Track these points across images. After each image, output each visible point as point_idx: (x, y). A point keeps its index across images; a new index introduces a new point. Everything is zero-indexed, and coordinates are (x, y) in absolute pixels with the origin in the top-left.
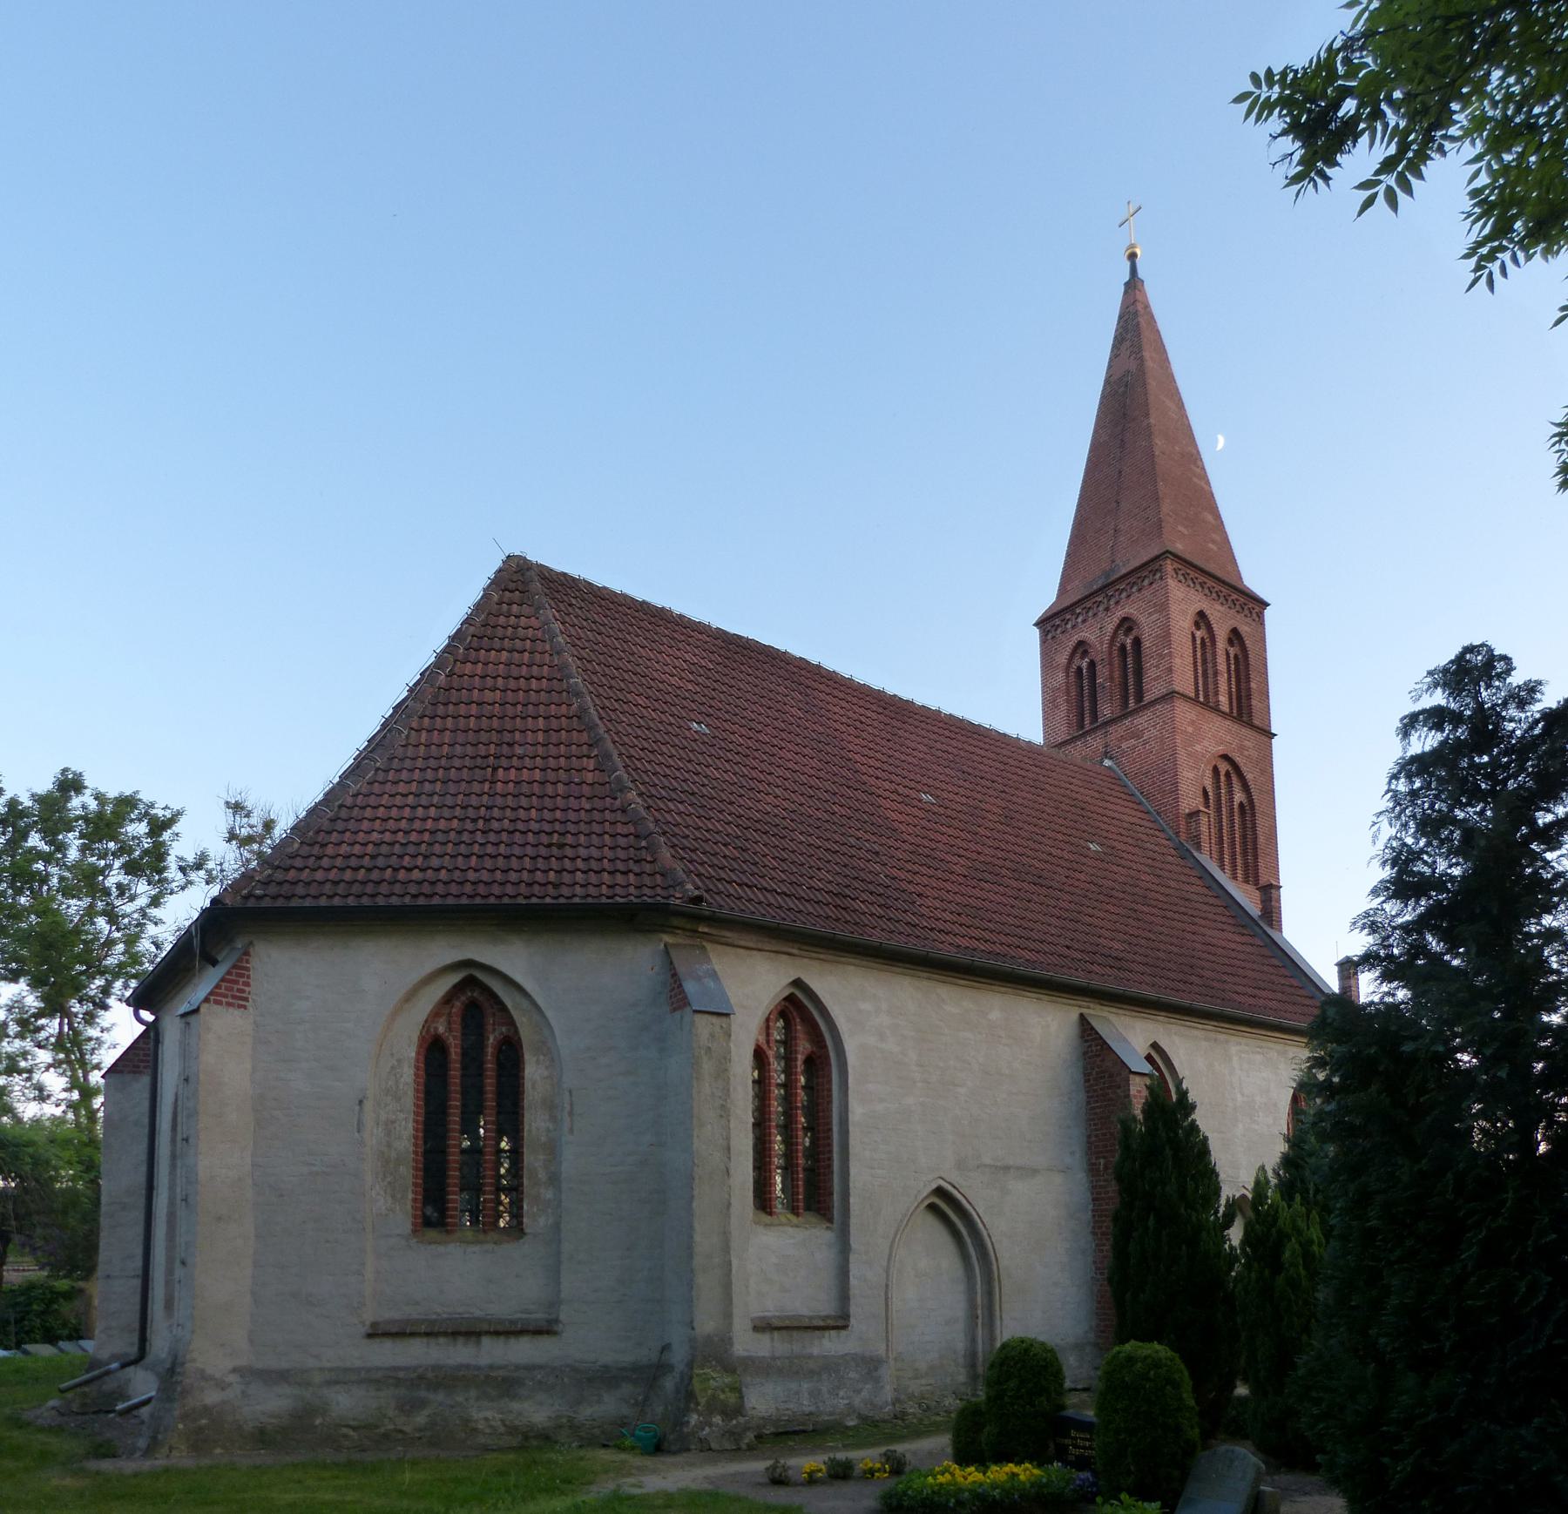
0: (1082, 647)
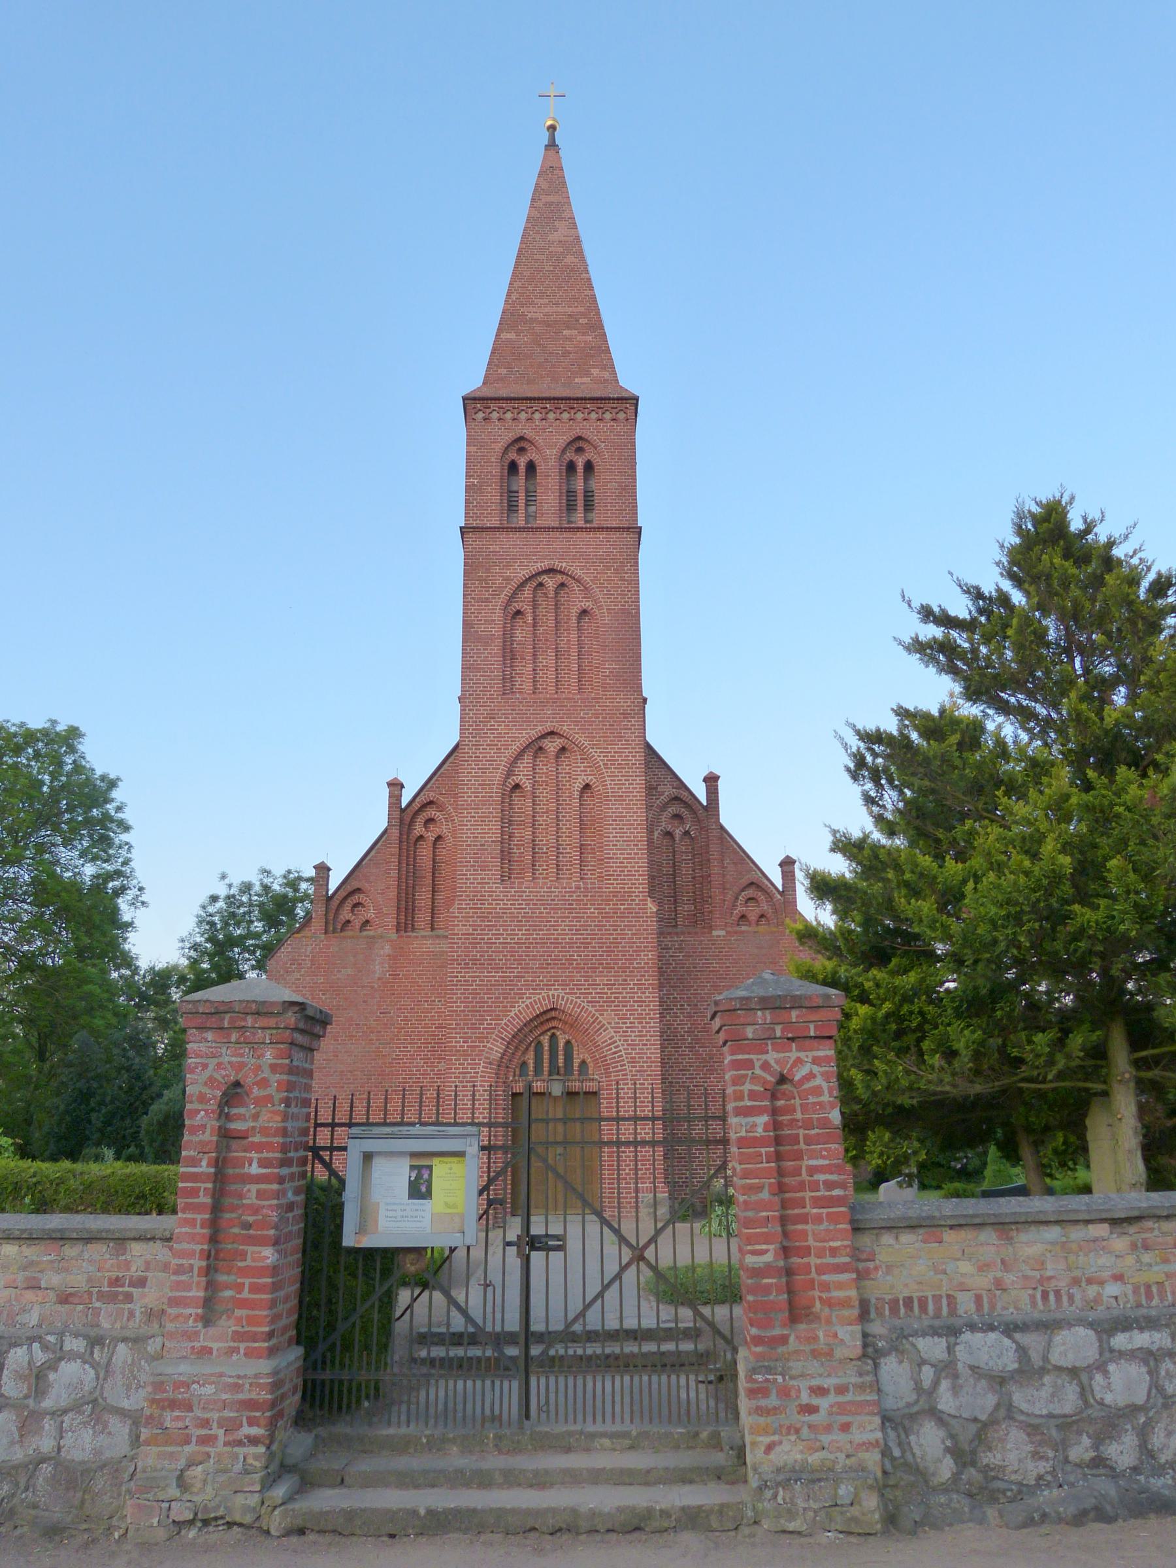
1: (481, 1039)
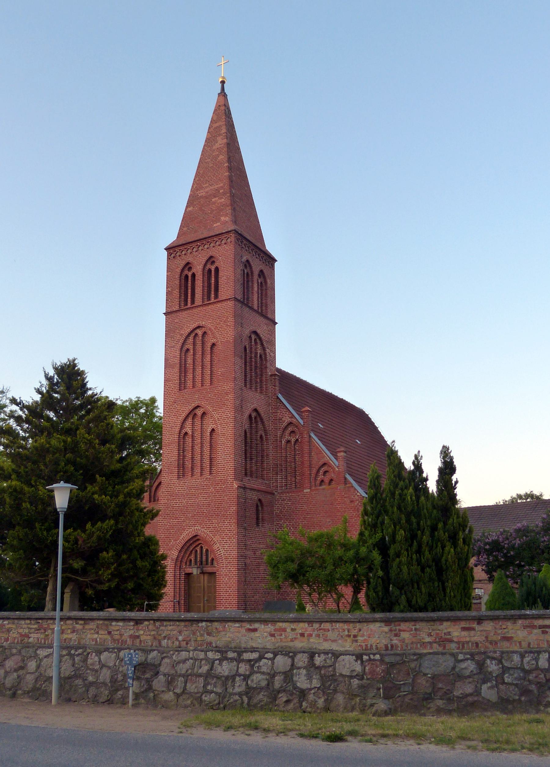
0: (188, 266)
1: (169, 550)
